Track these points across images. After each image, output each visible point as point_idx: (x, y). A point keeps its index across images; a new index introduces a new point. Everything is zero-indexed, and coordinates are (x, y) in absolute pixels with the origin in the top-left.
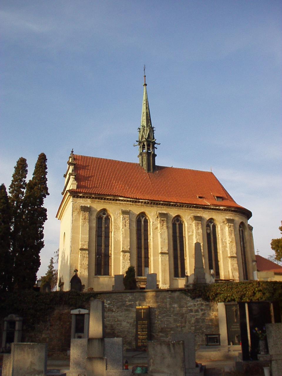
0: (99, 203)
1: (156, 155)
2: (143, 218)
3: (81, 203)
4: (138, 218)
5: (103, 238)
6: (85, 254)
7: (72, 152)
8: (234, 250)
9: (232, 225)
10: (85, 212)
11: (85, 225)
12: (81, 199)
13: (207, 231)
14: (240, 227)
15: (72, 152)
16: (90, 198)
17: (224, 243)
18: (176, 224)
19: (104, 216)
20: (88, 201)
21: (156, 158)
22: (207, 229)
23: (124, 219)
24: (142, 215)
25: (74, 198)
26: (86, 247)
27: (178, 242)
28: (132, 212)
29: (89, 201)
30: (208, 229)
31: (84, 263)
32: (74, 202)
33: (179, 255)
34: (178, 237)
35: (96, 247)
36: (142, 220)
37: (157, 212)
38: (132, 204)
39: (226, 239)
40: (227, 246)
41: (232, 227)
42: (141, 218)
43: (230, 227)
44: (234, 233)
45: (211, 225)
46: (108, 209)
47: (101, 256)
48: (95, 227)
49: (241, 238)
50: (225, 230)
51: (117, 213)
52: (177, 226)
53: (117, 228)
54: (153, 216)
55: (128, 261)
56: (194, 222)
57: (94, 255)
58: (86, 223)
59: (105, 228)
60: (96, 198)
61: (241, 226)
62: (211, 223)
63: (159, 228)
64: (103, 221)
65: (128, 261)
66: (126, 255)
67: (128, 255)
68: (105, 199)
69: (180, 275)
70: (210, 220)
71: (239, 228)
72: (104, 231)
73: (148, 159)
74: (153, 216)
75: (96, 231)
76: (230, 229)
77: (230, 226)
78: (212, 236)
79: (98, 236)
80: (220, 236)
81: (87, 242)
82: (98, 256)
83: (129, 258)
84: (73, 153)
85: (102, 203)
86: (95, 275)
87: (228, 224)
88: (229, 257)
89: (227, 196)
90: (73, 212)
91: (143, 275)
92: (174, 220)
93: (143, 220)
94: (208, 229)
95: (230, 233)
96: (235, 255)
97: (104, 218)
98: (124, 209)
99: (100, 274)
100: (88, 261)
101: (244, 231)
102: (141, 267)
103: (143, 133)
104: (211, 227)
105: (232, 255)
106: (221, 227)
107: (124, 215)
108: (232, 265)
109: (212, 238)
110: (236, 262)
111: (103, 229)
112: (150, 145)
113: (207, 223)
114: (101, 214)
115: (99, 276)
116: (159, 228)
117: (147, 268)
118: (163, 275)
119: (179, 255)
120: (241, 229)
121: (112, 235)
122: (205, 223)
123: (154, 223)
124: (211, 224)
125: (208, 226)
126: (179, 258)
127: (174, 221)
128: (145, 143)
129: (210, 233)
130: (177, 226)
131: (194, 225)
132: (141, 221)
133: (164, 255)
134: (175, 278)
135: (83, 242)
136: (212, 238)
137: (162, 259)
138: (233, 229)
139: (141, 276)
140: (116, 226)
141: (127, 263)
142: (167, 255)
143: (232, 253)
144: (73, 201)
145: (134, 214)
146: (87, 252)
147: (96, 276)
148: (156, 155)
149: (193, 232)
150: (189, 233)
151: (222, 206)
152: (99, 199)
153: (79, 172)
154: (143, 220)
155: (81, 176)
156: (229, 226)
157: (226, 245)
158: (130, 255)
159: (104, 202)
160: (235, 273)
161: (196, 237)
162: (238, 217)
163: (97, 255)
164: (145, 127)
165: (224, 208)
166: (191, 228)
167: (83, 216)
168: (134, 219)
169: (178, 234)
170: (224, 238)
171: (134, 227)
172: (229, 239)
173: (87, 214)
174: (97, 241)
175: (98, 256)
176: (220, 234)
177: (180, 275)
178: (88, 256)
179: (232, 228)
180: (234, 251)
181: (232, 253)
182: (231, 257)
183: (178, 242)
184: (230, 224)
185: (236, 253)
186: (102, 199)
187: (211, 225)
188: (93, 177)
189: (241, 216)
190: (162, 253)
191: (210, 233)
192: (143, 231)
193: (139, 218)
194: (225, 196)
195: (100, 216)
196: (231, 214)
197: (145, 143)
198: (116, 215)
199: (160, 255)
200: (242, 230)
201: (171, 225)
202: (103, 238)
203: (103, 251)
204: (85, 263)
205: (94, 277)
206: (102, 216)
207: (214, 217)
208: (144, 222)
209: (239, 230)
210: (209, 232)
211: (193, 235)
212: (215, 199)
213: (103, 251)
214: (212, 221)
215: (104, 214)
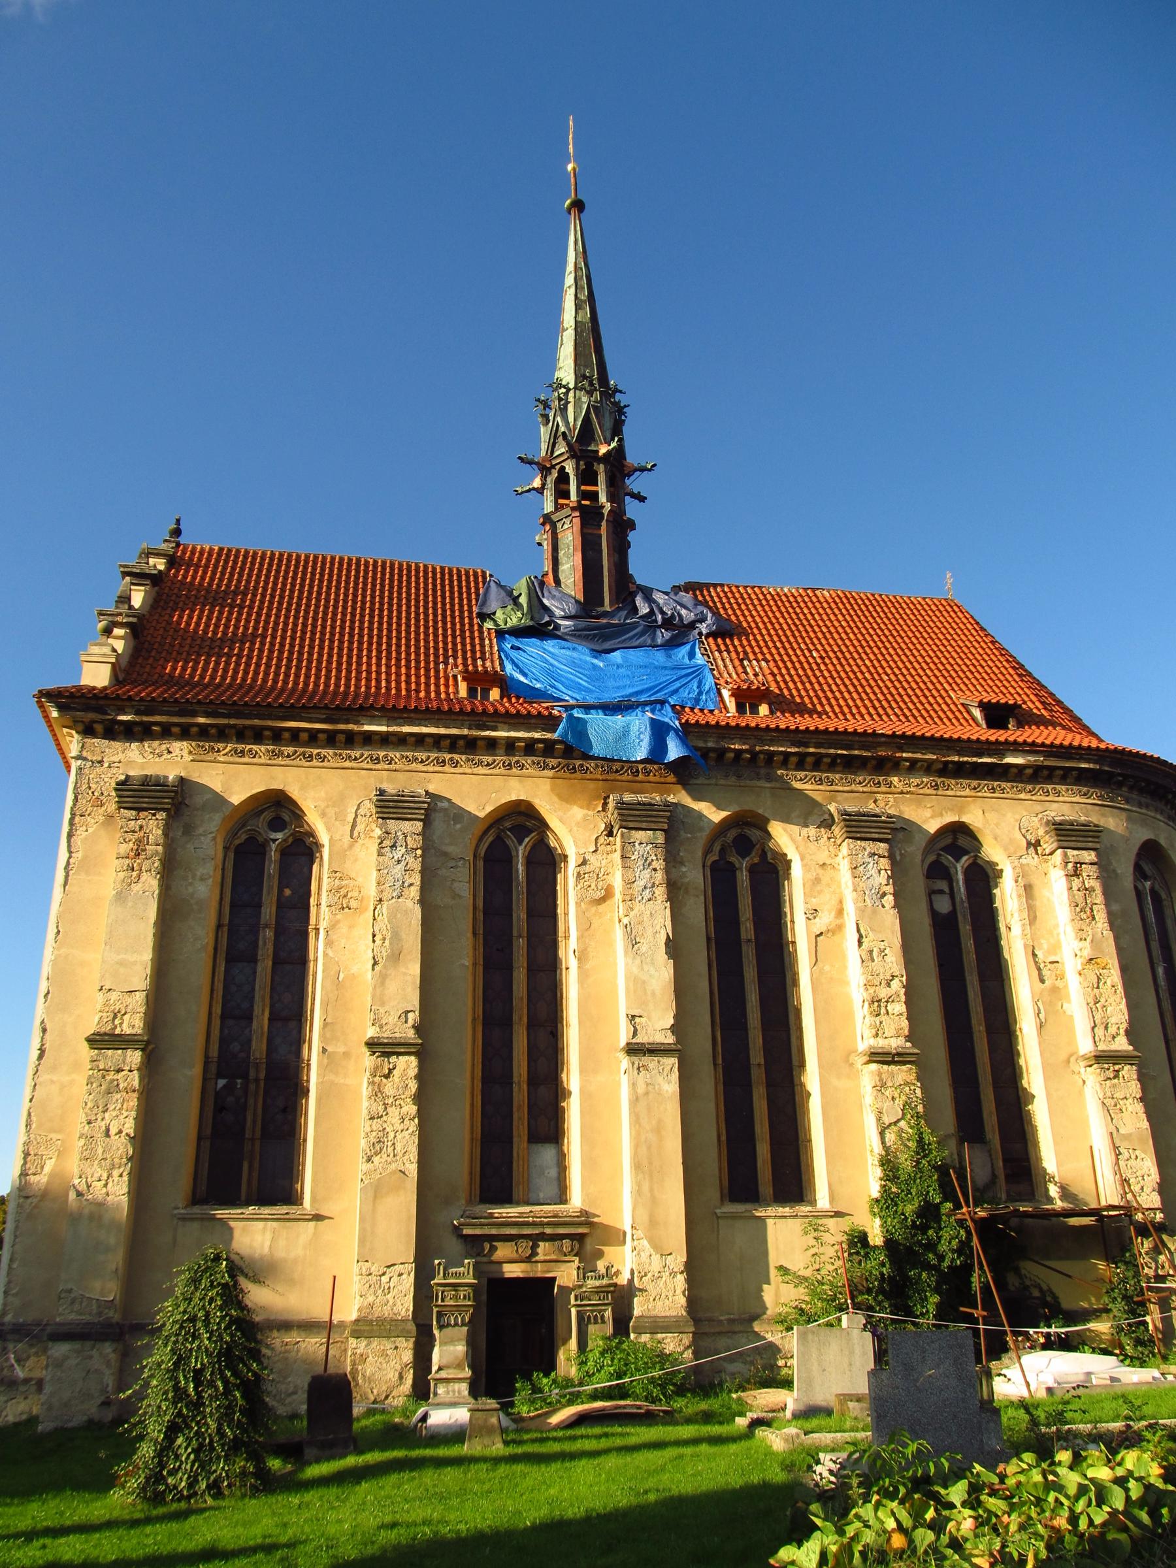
0: (246, 759)
1: (631, 525)
2: (520, 843)
3: (130, 763)
4: (490, 838)
5: (265, 966)
6: (119, 1070)
7: (177, 532)
8: (1118, 1013)
9: (1089, 856)
10: (143, 814)
11: (136, 888)
12: (134, 745)
13: (937, 907)
14: (1140, 872)
15: (177, 532)
16: (185, 734)
17: (1045, 972)
18: (732, 870)
19: (273, 835)
20: (177, 752)
21: (632, 536)
22: (931, 893)
23: (388, 843)
24: (521, 820)
25: (90, 741)
26: (133, 1024)
27: (750, 974)
28: (445, 804)
29: (181, 748)
30: (941, 892)
31: (108, 1130)
32: (85, 759)
33: (757, 1056)
34: (391, 729)
35: (217, 1023)
36: (514, 853)
37: (606, 798)
38: (451, 759)
39: (1055, 947)
40: (1066, 987)
41: (1088, 871)
42: (511, 841)
43: (1076, 873)
44: (1107, 905)
45: (959, 868)
46: (294, 793)
47: (245, 1077)
48: (214, 904)
49: (1155, 945)
50: (1045, 893)
51: (351, 818)
52: (743, 878)
53: (270, 888)
54: (578, 824)
55: (405, 1109)
56: (844, 849)
57: (197, 1071)
58: (145, 876)
59: (282, 905)
60: (222, 734)
61: (1147, 868)
62: (957, 852)
63: (618, 896)
64: (272, 867)
65: (405, 1109)
66: (390, 1071)
67: (407, 1065)
68: (277, 737)
69: (766, 1185)
70: (949, 840)
71: (1136, 879)
72: (267, 926)
73: (589, 546)
74: (578, 824)
75: (219, 926)
76: (1076, 883)
77: (1078, 864)
78: (965, 928)
79: (231, 960)
80: (1016, 930)
81: (140, 997)
82: (221, 1083)
83: (413, 1086)
84: (182, 540)
85: (263, 761)
86: (197, 1199)
87: (1065, 855)
88: (1085, 1058)
89: (1043, 703)
90: (77, 819)
91: (517, 1192)
92: (717, 847)
93: (521, 853)
94: (941, 892)
95: (1082, 911)
96: (1122, 1044)
97: (274, 846)
98: (391, 789)
99: (233, 1200)
100: (413, 1125)
101: (1163, 895)
102: (507, 1140)
103: (559, 419)
104: (960, 877)
105: (1102, 1047)
106: (1022, 874)
107: (392, 825)
108: (1110, 1109)
109: (968, 943)
110: (1135, 1088)
111: (269, 912)
112: (596, 474)
113: (932, 858)
114: (261, 823)
115: (221, 1213)
116: (618, 896)
117: (547, 1154)
118: (646, 1187)
119: (757, 1056)
120: (1148, 884)
121: (319, 950)
122: (915, 850)
123: (587, 868)
124: (958, 860)
125: (937, 871)
126: (758, 1075)
127: (723, 851)
128: (570, 467)
129: (953, 913)
130: (743, 878)
131: (844, 866)
132: (507, 860)
133: (651, 1062)
134: (739, 1208)
135: (114, 996)
136: (968, 943)
137: (634, 1085)
138: (1097, 885)
139: (507, 1199)
140: (343, 891)
141: (396, 1121)
142: (672, 1062)
143: (1100, 1031)
144: (85, 754)
145: (459, 814)
146: (135, 1057)
147: (197, 1210)
148: (631, 525)
149: (840, 912)
150: (756, 860)
151: (1016, 750)
152: (241, 735)
153: (181, 617)
154: (521, 853)
155: (181, 632)
156: (1070, 866)
157: (1059, 983)
158: (421, 1066)
159: (275, 755)
160: (1132, 1162)
161: (860, 943)
162: (1124, 815)
163: (220, 1075)
164: (569, 390)
165: (1031, 759)
166: (828, 885)
167: (129, 836)
168: (462, 847)
169: (747, 929)
170: (1045, 946)
171: (456, 896)
172: (1076, 945)
173: (154, 826)
174: (219, 987)
175: (221, 1083)
176: (1016, 915)
177: (766, 1185)
178: (136, 1083)
179: (1090, 877)
180: (1113, 1020)
181: (1100, 1031)
182: (1101, 1058)
183: (750, 974)
184: (1070, 852)
185: (1128, 1033)
186: (258, 736)
187: (959, 868)
188: (253, 644)
189: (1140, 805)
190: (633, 1050)
191: (953, 913)
192: (520, 914)
193: (499, 841)
194: (1033, 705)
195: (251, 840)
196: (1077, 799)
197: (570, 467)
198: (348, 828)
199: (625, 1061)
200: (1152, 890)
201: (695, 875)
202: (265, 966)
203: (259, 1048)
204: (113, 1131)
205: (183, 1219)
206: (260, 839)
207: (973, 817)
208: (529, 862)
209: (1139, 894)
210: (943, 905)
211: (840, 928)
212: (974, 719)
213: (259, 1048)
214: (962, 841)
215: (277, 824)
